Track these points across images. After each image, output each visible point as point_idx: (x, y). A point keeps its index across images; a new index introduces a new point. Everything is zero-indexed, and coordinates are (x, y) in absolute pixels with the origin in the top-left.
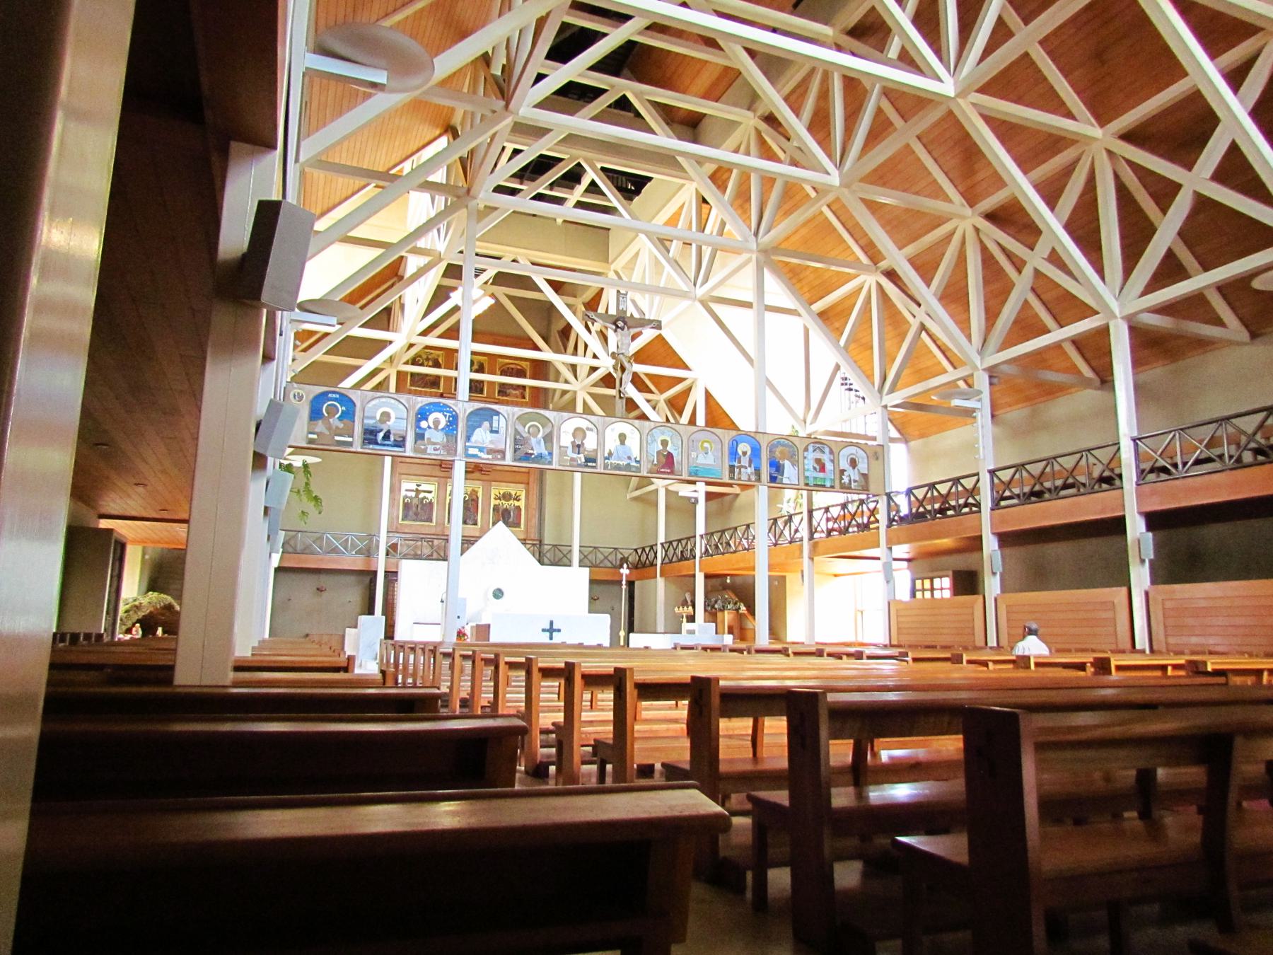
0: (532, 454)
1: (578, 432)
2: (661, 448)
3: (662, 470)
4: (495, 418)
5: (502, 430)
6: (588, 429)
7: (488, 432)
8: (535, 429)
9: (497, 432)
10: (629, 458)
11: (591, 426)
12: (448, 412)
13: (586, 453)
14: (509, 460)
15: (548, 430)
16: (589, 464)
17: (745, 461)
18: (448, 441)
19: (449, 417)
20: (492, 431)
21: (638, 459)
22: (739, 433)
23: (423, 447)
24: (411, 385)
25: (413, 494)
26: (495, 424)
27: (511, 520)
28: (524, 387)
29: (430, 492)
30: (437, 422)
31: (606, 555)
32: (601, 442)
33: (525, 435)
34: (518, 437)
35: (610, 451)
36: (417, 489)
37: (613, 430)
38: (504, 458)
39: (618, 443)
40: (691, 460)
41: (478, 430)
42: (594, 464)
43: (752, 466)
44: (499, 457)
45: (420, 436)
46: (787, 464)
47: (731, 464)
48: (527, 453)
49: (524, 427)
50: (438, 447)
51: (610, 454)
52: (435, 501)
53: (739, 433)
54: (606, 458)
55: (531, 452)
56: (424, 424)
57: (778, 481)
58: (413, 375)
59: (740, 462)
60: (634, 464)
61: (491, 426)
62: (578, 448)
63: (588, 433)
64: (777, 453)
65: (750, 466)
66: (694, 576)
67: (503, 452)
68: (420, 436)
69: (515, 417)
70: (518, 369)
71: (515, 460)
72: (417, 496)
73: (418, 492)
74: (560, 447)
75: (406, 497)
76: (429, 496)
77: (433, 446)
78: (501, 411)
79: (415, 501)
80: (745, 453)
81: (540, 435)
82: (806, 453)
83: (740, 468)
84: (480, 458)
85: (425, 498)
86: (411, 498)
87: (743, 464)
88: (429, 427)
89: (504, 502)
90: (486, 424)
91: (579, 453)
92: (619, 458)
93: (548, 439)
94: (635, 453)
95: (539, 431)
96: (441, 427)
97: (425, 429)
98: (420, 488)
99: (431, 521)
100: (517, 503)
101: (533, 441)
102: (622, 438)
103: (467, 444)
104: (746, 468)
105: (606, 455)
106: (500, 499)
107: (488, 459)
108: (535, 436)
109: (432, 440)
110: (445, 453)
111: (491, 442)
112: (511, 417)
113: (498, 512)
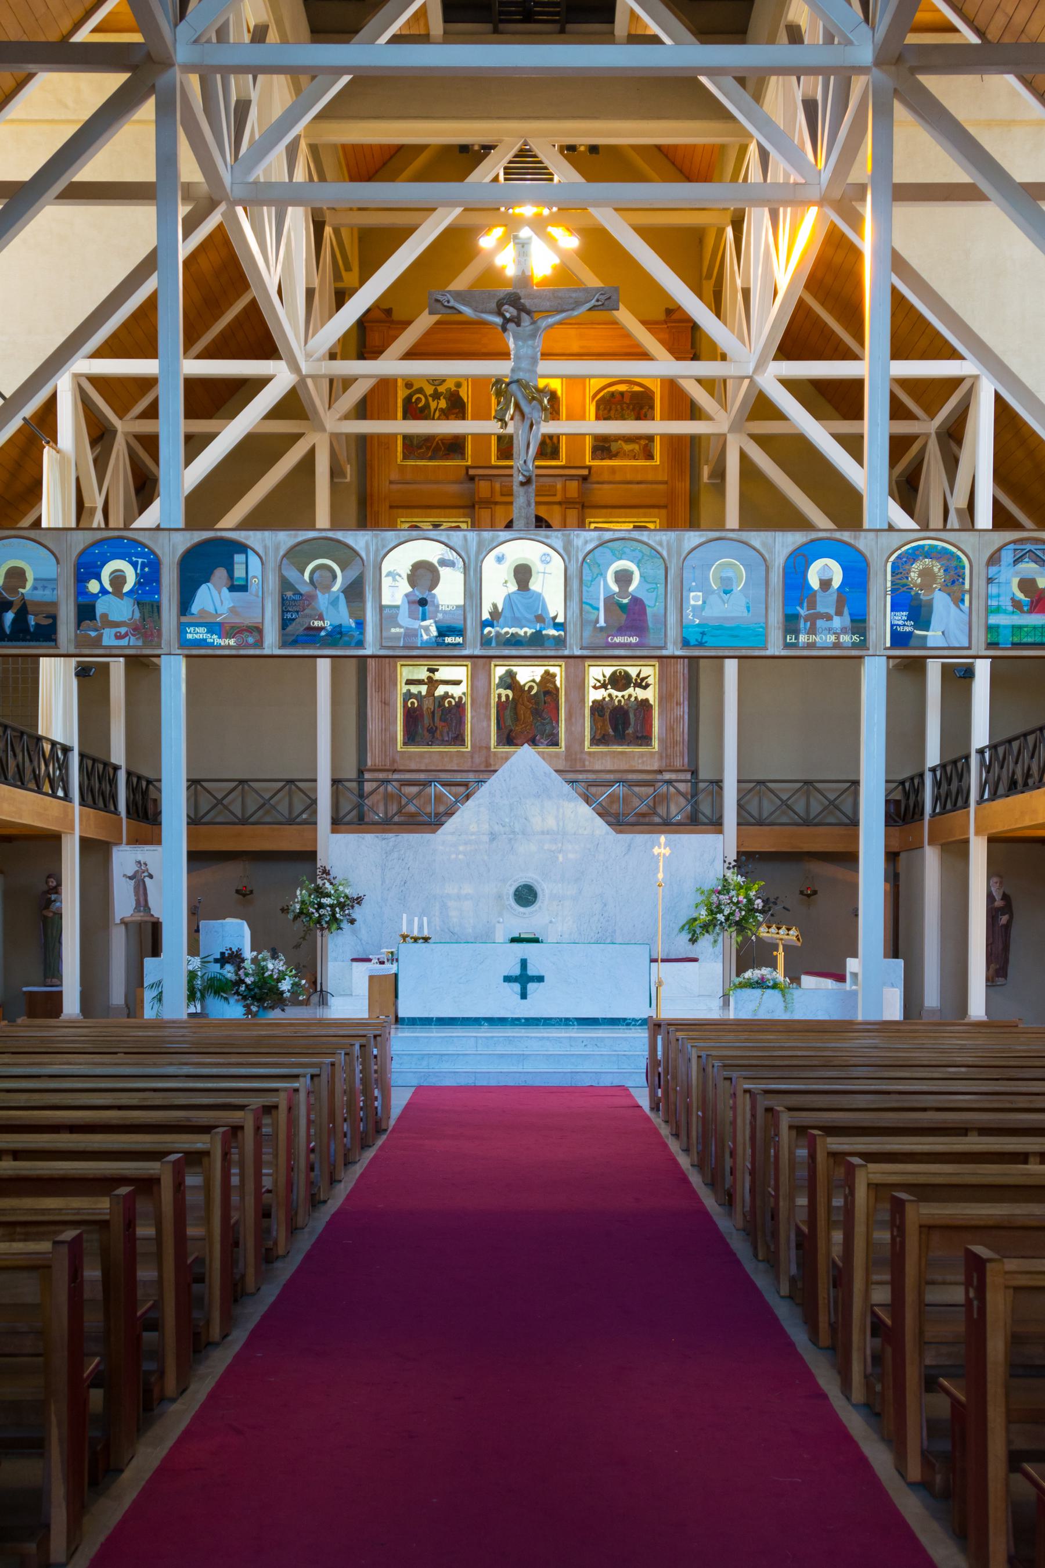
0: (321, 629)
1: (421, 571)
2: (615, 588)
3: (618, 640)
4: (239, 558)
5: (255, 583)
6: (443, 563)
7: (225, 590)
8: (329, 574)
9: (244, 588)
10: (540, 619)
11: (451, 556)
12: (138, 555)
13: (440, 616)
14: (271, 643)
15: (353, 574)
16: (448, 640)
17: (826, 604)
18: (143, 618)
19: (143, 565)
20: (233, 588)
21: (560, 619)
22: (814, 535)
23: (93, 634)
24: (405, 457)
25: (424, 689)
26: (239, 572)
27: (630, 731)
28: (650, 438)
29: (457, 683)
30: (118, 579)
31: (832, 797)
32: (473, 590)
33: (304, 589)
34: (289, 594)
35: (495, 606)
36: (429, 678)
37: (500, 559)
38: (260, 643)
39: (513, 587)
40: (689, 614)
41: (204, 587)
42: (460, 640)
43: (846, 611)
44: (251, 640)
45: (86, 612)
46: (941, 602)
47: (790, 611)
48: (310, 628)
49: (302, 572)
50: (123, 630)
51: (495, 614)
52: (467, 701)
53: (814, 535)
54: (485, 624)
55: (317, 623)
56: (93, 586)
57: (913, 642)
58: (407, 438)
59: (812, 605)
60: (552, 632)
61: (231, 575)
62: (422, 603)
63: (444, 572)
64: (913, 575)
65: (839, 613)
66: (966, 842)
67: (258, 630)
68: (86, 612)
69: (282, 553)
70: (635, 394)
71: (284, 645)
72: (431, 692)
73: (432, 683)
74: (381, 608)
75: (409, 695)
76: (456, 691)
77: (114, 631)
78: (249, 543)
79: (428, 704)
80: (826, 584)
81: (337, 587)
82: (993, 570)
83: (813, 619)
84: (211, 646)
85: (446, 695)
86: (418, 696)
87: (821, 609)
88: (103, 591)
89: (614, 693)
90: (220, 573)
91: (424, 619)
92: (518, 623)
93: (355, 592)
94: (555, 606)
95: (335, 577)
96: (127, 588)
97: (96, 596)
98: (437, 676)
99: (462, 743)
100: (641, 694)
101: (322, 601)
102: (523, 574)
103: (184, 619)
104: (829, 618)
105: (486, 616)
106: (604, 686)
107: (229, 647)
108: (327, 588)
109: (111, 618)
110: (140, 643)
111: (232, 610)
112: (271, 553)
113: (602, 716)
